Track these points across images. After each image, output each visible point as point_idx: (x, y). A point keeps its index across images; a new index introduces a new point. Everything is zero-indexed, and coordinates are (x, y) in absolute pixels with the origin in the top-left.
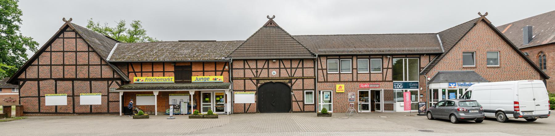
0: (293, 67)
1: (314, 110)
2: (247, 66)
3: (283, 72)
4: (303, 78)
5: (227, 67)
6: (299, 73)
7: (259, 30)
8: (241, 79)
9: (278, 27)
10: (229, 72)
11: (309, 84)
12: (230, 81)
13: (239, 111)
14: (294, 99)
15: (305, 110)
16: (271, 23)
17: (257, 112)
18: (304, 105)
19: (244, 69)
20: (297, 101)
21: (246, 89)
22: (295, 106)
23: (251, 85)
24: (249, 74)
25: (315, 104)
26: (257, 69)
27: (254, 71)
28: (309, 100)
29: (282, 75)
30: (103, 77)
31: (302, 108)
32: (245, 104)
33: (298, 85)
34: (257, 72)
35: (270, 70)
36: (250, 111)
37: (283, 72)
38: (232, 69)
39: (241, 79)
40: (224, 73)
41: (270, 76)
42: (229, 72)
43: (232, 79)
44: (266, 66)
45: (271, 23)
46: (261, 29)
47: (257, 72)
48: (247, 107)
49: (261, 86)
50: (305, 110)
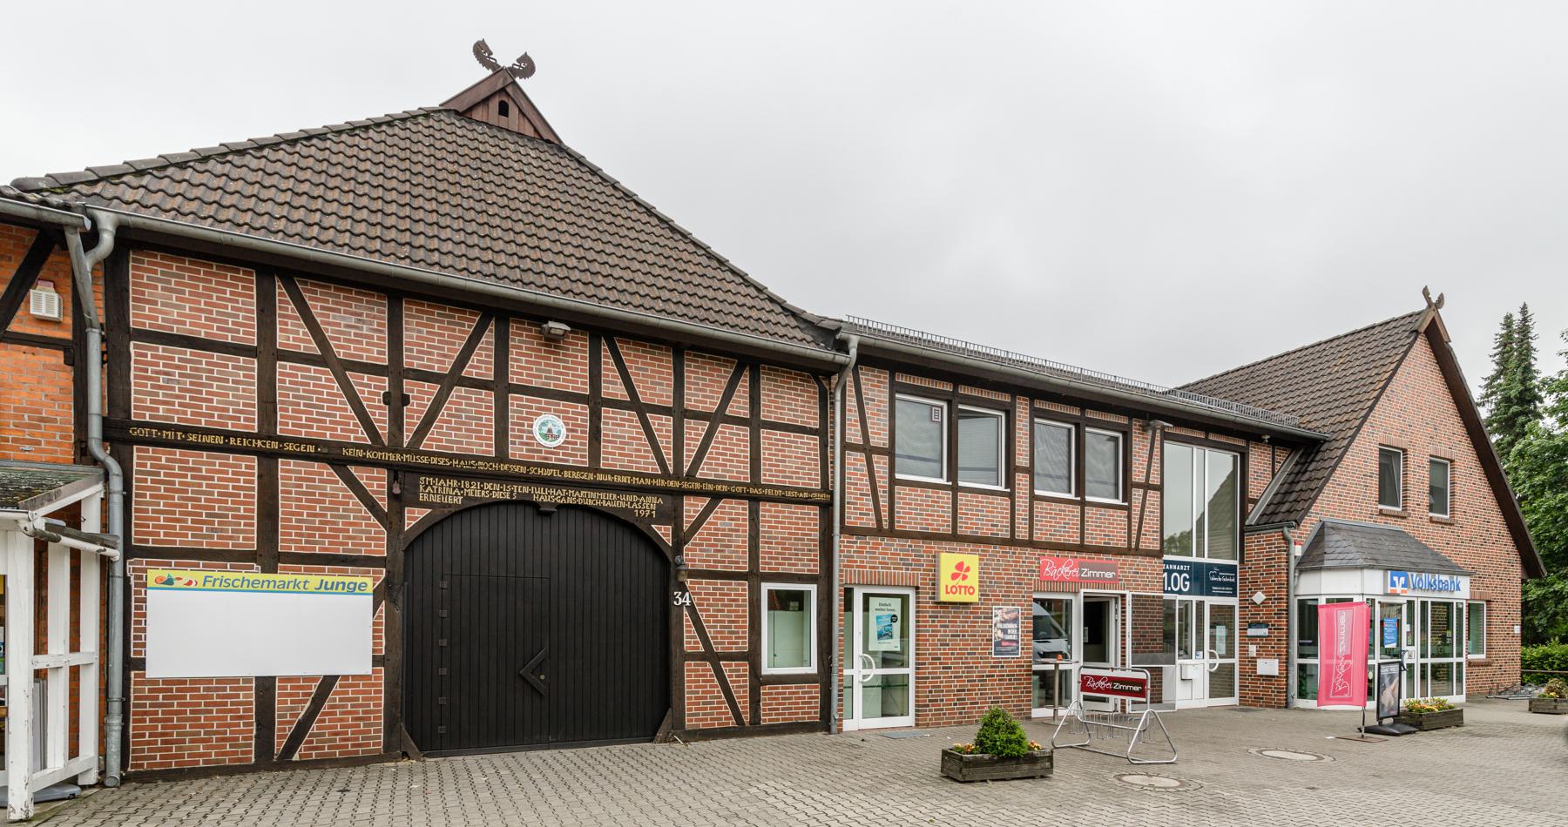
1: (814, 715)
3: (620, 428)
5: (44, 302)
7: (413, 117)
8: (227, 443)
11: (789, 534)
12: (82, 452)
13: (202, 753)
14: (690, 641)
15: (765, 720)
16: (500, 99)
17: (393, 750)
20: (711, 656)
21: (287, 542)
22: (699, 693)
27: (371, 390)
28: (784, 651)
30: (815, 568)
31: (743, 704)
32: (265, 686)
33: (717, 538)
34: (397, 401)
35: (515, 401)
37: (620, 428)
38: (119, 333)
39: (227, 443)
41: (516, 451)
42: (75, 354)
45: (500, 99)
47: (397, 401)
49: (429, 530)
50: (765, 720)
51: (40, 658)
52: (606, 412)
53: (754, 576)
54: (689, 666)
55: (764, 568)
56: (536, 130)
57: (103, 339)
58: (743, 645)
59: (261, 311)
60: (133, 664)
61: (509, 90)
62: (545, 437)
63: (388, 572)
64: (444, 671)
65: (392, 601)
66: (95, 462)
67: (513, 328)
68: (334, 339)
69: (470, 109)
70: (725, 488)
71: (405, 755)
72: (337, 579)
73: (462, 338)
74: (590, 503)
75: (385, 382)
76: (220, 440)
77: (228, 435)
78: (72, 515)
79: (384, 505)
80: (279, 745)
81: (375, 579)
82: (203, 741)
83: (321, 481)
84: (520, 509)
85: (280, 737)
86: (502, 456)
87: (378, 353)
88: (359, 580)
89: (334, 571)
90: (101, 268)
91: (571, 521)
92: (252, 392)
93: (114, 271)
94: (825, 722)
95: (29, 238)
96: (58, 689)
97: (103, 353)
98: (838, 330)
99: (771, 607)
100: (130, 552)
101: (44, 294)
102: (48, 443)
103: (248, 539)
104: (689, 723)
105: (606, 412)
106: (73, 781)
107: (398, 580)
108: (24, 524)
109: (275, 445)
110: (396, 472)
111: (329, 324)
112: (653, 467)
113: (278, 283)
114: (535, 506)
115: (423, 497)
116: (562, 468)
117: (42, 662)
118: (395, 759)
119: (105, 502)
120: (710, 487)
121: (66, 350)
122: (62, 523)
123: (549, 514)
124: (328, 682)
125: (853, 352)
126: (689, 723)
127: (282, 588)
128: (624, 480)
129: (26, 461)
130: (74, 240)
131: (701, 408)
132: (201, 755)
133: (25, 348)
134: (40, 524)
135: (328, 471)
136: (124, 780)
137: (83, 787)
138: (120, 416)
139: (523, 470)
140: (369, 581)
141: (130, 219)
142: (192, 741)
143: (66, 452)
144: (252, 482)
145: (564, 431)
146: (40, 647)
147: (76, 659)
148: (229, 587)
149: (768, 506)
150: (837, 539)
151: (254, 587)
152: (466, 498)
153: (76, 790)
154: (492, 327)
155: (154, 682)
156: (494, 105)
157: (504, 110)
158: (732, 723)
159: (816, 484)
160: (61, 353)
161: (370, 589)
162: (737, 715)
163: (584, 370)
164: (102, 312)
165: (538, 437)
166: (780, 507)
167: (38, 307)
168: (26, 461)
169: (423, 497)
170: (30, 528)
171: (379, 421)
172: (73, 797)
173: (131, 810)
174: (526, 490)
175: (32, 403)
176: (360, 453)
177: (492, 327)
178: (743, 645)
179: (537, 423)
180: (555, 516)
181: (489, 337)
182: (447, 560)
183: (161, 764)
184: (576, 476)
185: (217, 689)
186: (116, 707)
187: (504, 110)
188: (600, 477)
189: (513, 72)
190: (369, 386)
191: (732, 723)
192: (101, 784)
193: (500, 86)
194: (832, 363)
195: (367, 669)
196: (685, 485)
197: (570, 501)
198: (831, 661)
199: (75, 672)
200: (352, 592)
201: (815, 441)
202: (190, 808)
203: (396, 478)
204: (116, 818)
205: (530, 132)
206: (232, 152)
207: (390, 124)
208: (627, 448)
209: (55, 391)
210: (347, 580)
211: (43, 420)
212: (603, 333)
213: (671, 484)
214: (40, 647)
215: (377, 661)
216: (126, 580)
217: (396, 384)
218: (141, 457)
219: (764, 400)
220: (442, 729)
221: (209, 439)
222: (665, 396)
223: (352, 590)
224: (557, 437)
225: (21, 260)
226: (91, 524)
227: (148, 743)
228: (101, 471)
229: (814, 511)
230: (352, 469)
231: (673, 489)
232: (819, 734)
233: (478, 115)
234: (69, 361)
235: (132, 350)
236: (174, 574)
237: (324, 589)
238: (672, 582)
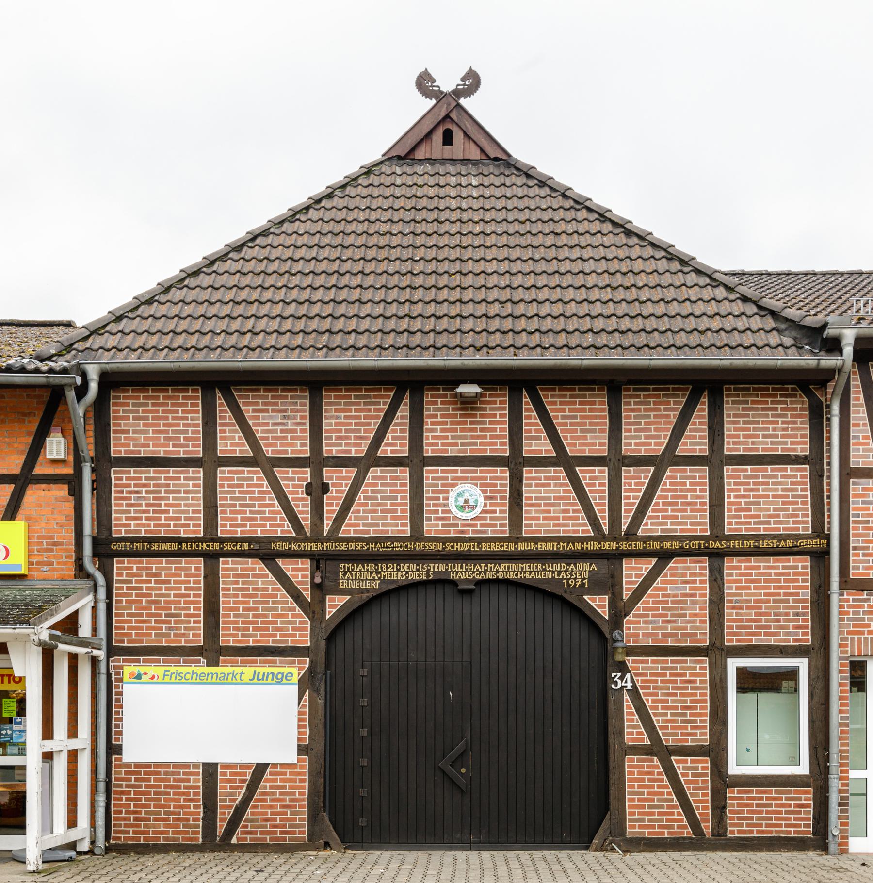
0: (631, 446)
1: (805, 828)
2: (231, 441)
3: (545, 488)
4: (715, 550)
5: (56, 447)
6: (679, 507)
7: (353, 181)
8: (179, 548)
9: (504, 162)
10: (76, 492)
11: (768, 599)
12: (81, 571)
13: (161, 831)
14: (633, 731)
15: (733, 831)
16: (447, 130)
17: (317, 840)
18: (722, 782)
19: (210, 461)
20: (658, 749)
21: (228, 638)
22: (643, 793)
23: (262, 603)
24: (250, 506)
25: (819, 778)
26: (317, 461)
27: (294, 481)
28: (764, 743)
29: (535, 523)
30: (806, 637)
31: (703, 810)
32: (210, 771)
33: (668, 606)
34: (317, 490)
35: (430, 474)
36: (258, 822)
37: (545, 488)
38: (104, 461)
39: (179, 548)
40: (34, 495)
41: (431, 528)
42: (74, 484)
43: (106, 549)
44: (396, 443)
45: (447, 130)
46: (368, 171)
47: (317, 490)
48: (229, 795)
49: (350, 617)
50: (733, 831)
51: (47, 742)
52: (529, 473)
53: (716, 651)
54: (631, 762)
55: (730, 640)
56: (482, 151)
57: (93, 470)
58: (703, 737)
59: (205, 424)
60: (113, 749)
61: (453, 116)
62: (462, 508)
63: (311, 661)
64: (364, 762)
65: (315, 691)
66: (89, 576)
67: (428, 397)
68: (263, 438)
69: (413, 149)
70: (676, 545)
71: (327, 845)
72: (268, 670)
73: (377, 417)
74: (512, 576)
75: (307, 474)
76: (174, 547)
77: (180, 541)
78: (70, 625)
79: (307, 595)
80: (221, 827)
81: (300, 669)
82: (163, 820)
83: (254, 576)
84: (439, 589)
85: (222, 820)
86: (417, 534)
87: (301, 447)
88: (286, 670)
89: (265, 662)
90: (91, 409)
91: (494, 598)
92: (198, 499)
93: (100, 412)
94: (819, 839)
95: (46, 395)
96: (61, 765)
97: (93, 482)
98: (825, 326)
99: (742, 689)
100: (112, 651)
101: (55, 439)
102: (58, 563)
103: (196, 636)
104: (632, 830)
105: (529, 473)
106: (72, 846)
107: (321, 668)
108: (33, 637)
109: (216, 546)
110: (318, 562)
111: (259, 425)
112: (584, 529)
113: (219, 395)
114: (454, 583)
115: (343, 584)
116: (480, 541)
117: (49, 746)
118: (317, 849)
119: (94, 609)
120: (656, 545)
121: (69, 483)
122: (58, 633)
123: (470, 592)
124: (260, 769)
125: (848, 350)
126: (632, 830)
127: (223, 680)
128: (550, 547)
129: (44, 580)
130: (71, 395)
131: (643, 451)
132: (162, 833)
133: (43, 486)
134: (45, 636)
135: (258, 566)
136: (108, 850)
137: (80, 854)
138: (104, 536)
139: (439, 546)
140: (294, 671)
141: (107, 366)
142: (155, 819)
143: (70, 569)
144: (199, 582)
145: (481, 500)
146: (48, 733)
147: (74, 744)
148: (181, 680)
149: (735, 561)
150: (835, 599)
151: (201, 680)
152: (383, 581)
153: (73, 854)
154: (406, 400)
155: (128, 765)
156: (438, 137)
157: (448, 139)
158: (687, 832)
159: (805, 527)
160: (66, 487)
161: (295, 679)
162: (694, 823)
163: (502, 429)
164: (92, 447)
165: (454, 510)
166: (753, 561)
167: (51, 453)
168: (44, 580)
169: (343, 584)
170: (37, 640)
171: (302, 512)
172: (71, 859)
173: (104, 872)
174: (443, 567)
175: (49, 531)
176: (286, 546)
177: (406, 400)
178: (703, 737)
179: (452, 495)
180: (477, 592)
181: (404, 411)
182: (368, 646)
183: (133, 839)
184: (495, 547)
185: (173, 773)
186: (102, 786)
187: (448, 139)
188: (522, 547)
189: (458, 93)
190: (292, 479)
191: (687, 832)
192: (91, 852)
193: (443, 114)
194: (818, 370)
195: (292, 757)
196: (624, 546)
197: (489, 576)
198: (827, 758)
199: (73, 755)
200: (279, 682)
201: (805, 470)
202: (143, 874)
203: (318, 567)
204: (93, 877)
205: (475, 154)
206: (189, 275)
207: (330, 196)
208: (554, 509)
209: (62, 519)
210: (276, 670)
211: (55, 544)
212: (522, 385)
213: (606, 546)
214: (48, 733)
215: (302, 750)
216: (109, 675)
217: (318, 474)
218: (119, 566)
219: (728, 429)
220: (363, 822)
221: (167, 547)
222: (596, 442)
223: (280, 680)
224: (474, 508)
225: (41, 414)
226: (85, 630)
227: (124, 819)
228: (92, 583)
229: (804, 564)
230: (280, 562)
231: (606, 556)
232: (811, 854)
233: (420, 154)
234: (71, 493)
235: (113, 476)
236: (142, 670)
237: (257, 679)
238: (610, 661)
